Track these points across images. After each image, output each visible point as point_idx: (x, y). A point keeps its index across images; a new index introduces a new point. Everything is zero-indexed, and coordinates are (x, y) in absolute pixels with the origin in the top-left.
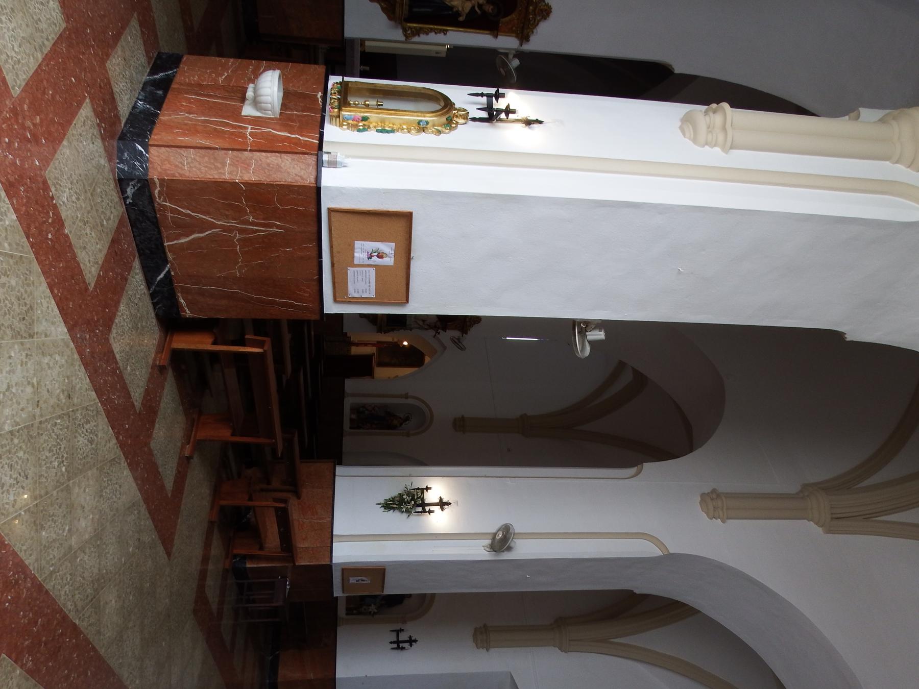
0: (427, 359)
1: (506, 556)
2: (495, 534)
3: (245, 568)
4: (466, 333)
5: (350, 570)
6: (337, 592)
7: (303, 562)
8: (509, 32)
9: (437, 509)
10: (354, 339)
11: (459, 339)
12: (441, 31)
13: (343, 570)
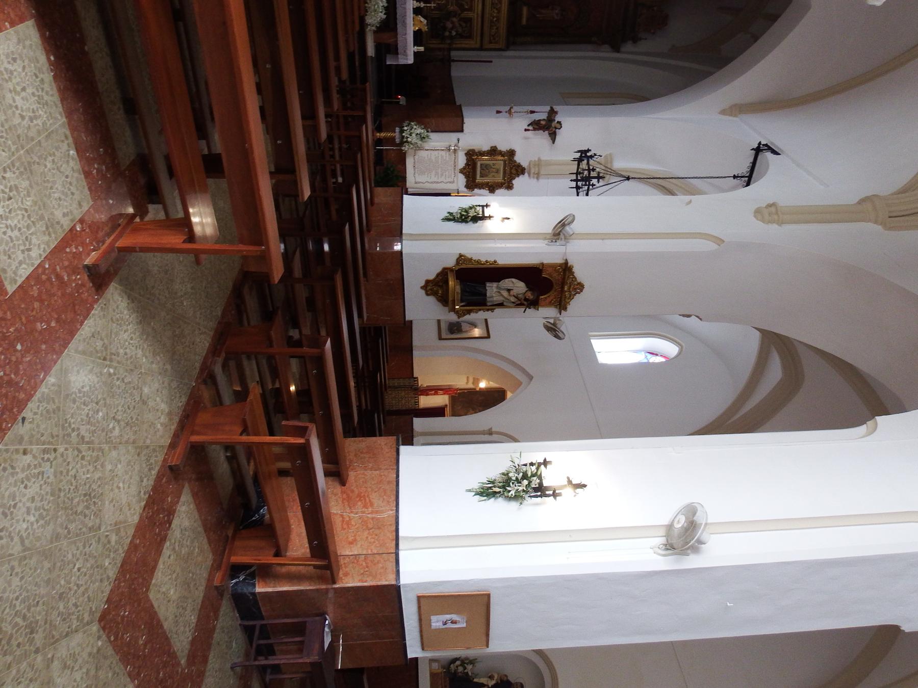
0: (509, 395)
1: (692, 562)
2: (670, 527)
3: (254, 594)
4: (565, 309)
5: (431, 602)
6: (413, 650)
7: (350, 579)
8: (550, 304)
9: (568, 492)
10: (424, 381)
11: (554, 324)
13: (419, 598)
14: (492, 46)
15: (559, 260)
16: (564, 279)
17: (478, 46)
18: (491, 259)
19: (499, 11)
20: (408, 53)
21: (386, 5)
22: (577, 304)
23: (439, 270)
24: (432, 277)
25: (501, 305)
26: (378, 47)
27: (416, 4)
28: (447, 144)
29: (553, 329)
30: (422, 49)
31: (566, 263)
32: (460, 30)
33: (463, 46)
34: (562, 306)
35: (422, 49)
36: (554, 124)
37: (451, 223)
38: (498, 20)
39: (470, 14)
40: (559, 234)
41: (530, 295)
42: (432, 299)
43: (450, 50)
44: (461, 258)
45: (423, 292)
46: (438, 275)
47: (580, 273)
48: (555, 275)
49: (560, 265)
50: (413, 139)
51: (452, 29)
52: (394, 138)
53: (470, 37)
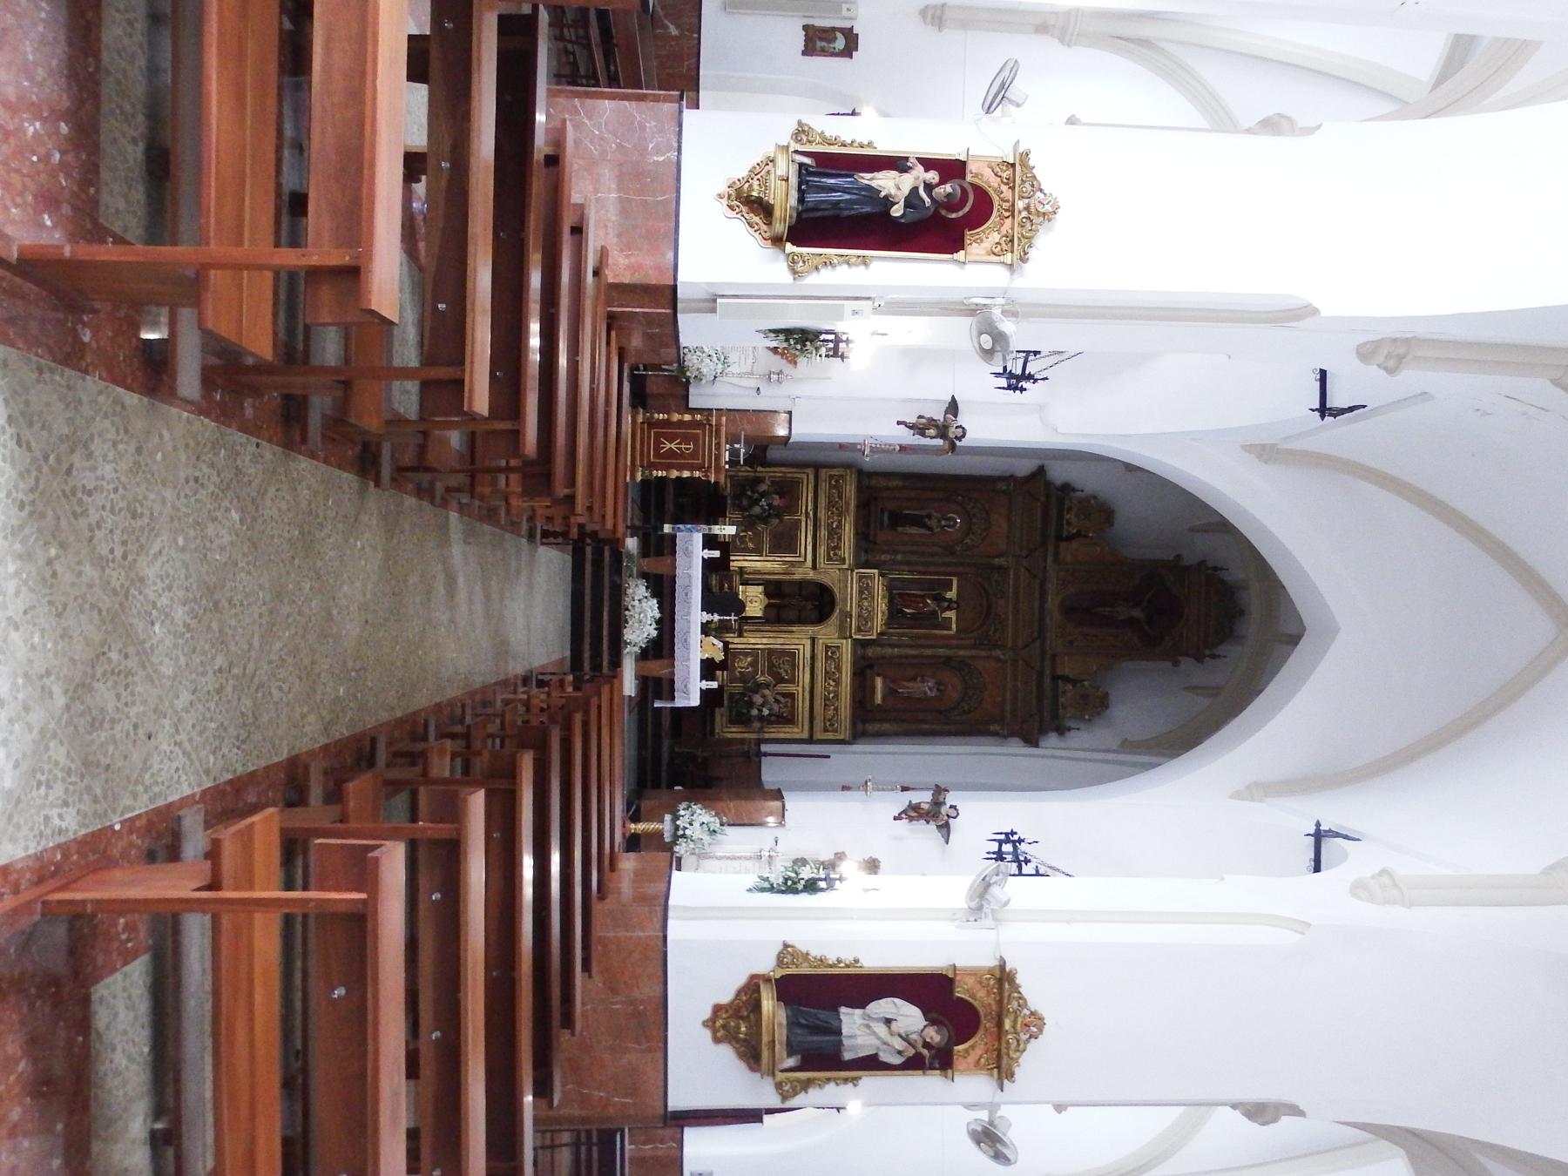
4: (1011, 1076)
12: (846, 1080)
14: (830, 736)
15: (988, 961)
16: (1000, 1003)
17: (805, 735)
18: (848, 957)
19: (838, 682)
20: (691, 691)
21: (658, 615)
22: (1032, 1062)
23: (741, 980)
24: (726, 997)
25: (872, 1064)
26: (644, 682)
27: (706, 617)
28: (756, 848)
29: (989, 1138)
30: (716, 554)
31: (1002, 966)
32: (776, 707)
33: (782, 736)
34: (1001, 1067)
35: (714, 685)
36: (944, 810)
37: (767, 895)
38: (836, 696)
39: (791, 688)
40: (980, 908)
41: (934, 1036)
42: (726, 1053)
43: (759, 742)
44: (787, 953)
45: (708, 1034)
46: (739, 993)
47: (1034, 990)
48: (981, 994)
49: (990, 971)
50: (695, 831)
51: (763, 705)
52: (660, 834)
53: (790, 720)
